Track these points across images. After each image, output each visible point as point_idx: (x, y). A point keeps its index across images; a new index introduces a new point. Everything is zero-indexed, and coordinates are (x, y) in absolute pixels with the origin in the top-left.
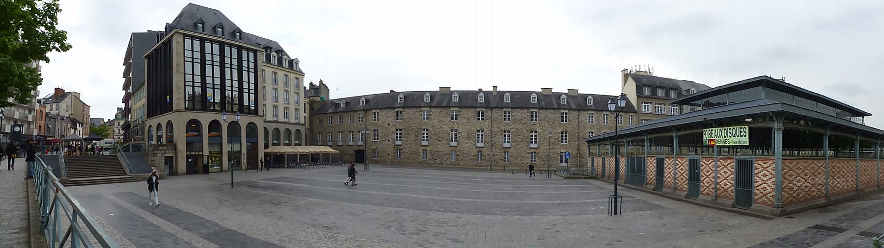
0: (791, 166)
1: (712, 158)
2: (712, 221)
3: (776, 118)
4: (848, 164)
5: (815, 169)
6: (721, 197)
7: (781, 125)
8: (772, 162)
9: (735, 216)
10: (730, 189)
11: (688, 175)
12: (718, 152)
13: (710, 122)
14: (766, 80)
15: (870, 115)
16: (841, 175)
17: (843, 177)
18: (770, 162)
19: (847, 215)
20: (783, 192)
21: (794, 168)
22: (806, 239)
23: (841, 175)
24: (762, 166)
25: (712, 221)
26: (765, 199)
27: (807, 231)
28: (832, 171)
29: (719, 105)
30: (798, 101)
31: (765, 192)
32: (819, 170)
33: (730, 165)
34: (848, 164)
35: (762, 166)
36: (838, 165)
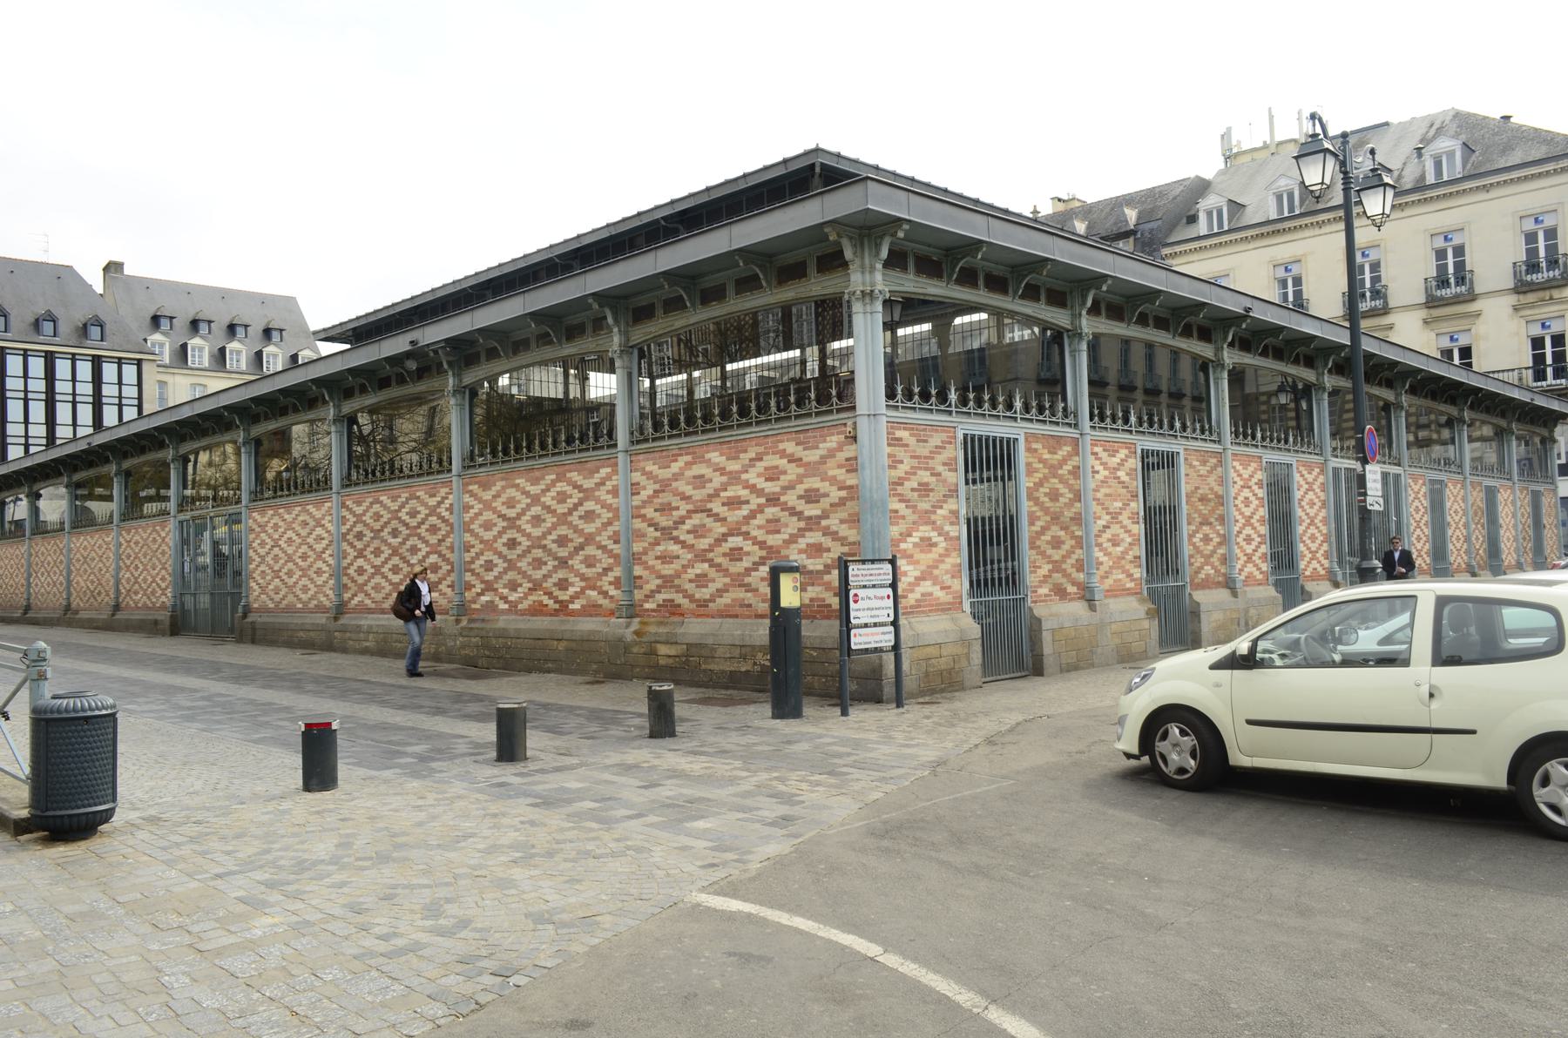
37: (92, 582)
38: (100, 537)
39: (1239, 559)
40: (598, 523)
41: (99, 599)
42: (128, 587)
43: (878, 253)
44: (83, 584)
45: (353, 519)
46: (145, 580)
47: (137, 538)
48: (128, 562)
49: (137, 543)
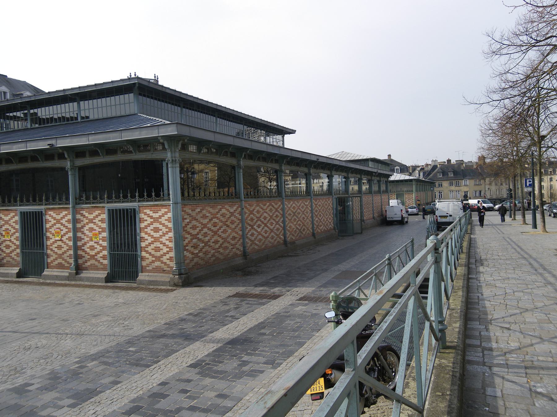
0: (194, 214)
1: (66, 208)
2: (79, 304)
3: (169, 146)
4: (271, 207)
5: (227, 216)
6: (86, 269)
7: (177, 155)
8: (221, 207)
9: (114, 293)
10: (101, 255)
11: (20, 239)
12: (76, 199)
13: (61, 151)
14: (139, 84)
15: (292, 132)
16: (263, 222)
17: (266, 225)
18: (164, 210)
19: (277, 276)
20: (185, 252)
21: (198, 217)
22: (229, 311)
23: (263, 222)
24: (151, 217)
25: (79, 304)
26: (157, 264)
27: (227, 301)
28: (249, 218)
29: (48, 123)
30: (203, 120)
31: (158, 254)
32: (233, 218)
33: (100, 218)
34: (271, 207)
35: (151, 217)
36: (258, 208)
37: (300, 225)
38: (302, 202)
39: (248, 243)
40: (161, 233)
41: (304, 233)
42: (317, 224)
43: (177, 146)
44: (293, 227)
45: (267, 211)
46: (324, 220)
47: (320, 203)
48: (316, 214)
49: (319, 205)
